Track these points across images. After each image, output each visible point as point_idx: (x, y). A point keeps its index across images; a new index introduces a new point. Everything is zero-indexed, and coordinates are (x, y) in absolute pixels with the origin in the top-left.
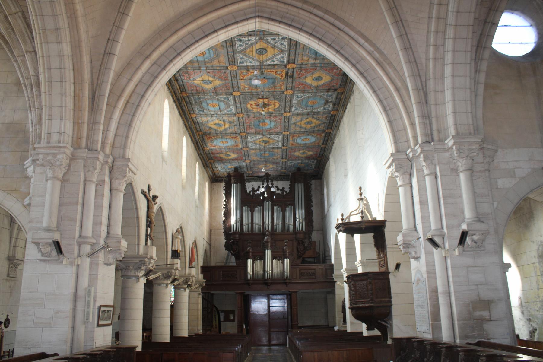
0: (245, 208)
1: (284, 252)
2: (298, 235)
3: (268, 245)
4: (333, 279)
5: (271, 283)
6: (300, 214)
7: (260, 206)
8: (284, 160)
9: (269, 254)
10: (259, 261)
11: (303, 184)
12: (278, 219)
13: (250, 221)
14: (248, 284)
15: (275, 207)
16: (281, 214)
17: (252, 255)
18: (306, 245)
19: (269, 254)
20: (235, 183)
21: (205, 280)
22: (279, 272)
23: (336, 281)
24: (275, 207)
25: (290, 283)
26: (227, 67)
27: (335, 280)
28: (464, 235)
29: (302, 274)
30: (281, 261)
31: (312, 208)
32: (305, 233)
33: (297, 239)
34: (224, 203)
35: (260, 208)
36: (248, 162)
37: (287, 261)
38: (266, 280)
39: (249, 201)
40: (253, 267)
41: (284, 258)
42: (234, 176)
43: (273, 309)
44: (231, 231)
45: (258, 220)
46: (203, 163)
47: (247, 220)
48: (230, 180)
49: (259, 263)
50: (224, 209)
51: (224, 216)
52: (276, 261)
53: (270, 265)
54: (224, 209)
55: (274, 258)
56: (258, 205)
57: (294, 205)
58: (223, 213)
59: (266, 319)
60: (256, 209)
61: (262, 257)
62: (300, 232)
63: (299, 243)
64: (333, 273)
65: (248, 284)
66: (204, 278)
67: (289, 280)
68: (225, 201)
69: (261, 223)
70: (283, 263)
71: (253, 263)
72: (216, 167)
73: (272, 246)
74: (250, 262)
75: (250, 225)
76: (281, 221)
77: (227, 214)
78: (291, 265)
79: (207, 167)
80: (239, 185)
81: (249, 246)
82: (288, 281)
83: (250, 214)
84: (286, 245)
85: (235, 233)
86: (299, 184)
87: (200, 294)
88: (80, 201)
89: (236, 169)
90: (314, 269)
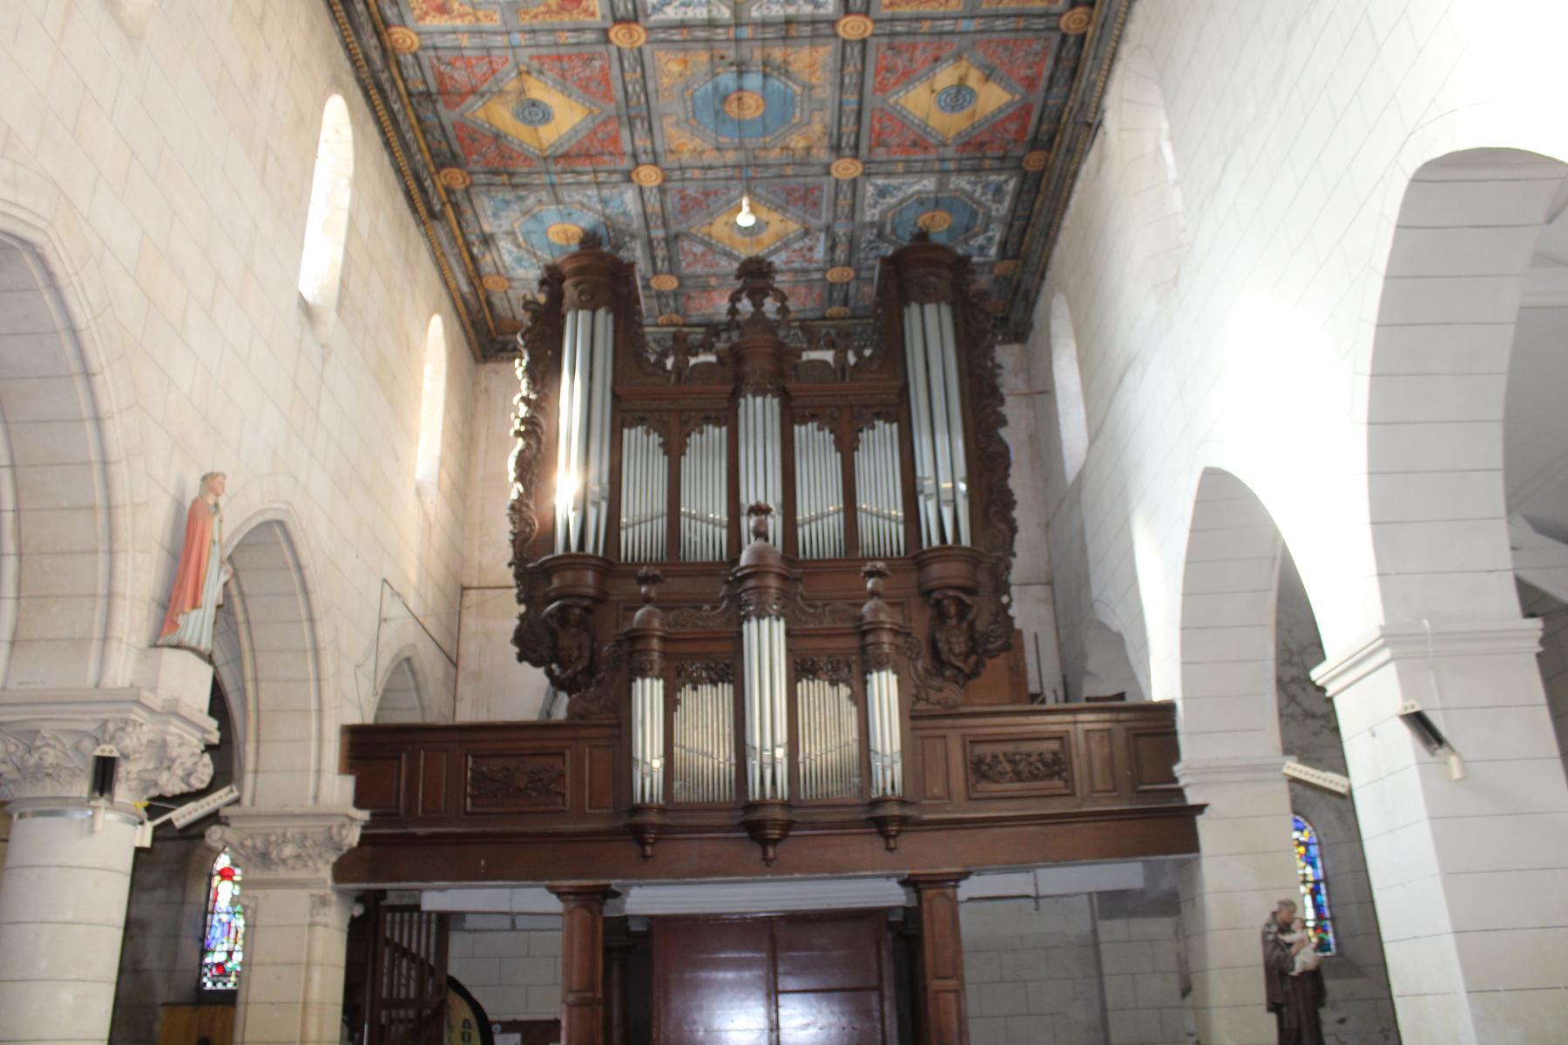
0: (634, 437)
1: (864, 631)
2: (936, 570)
3: (761, 590)
4: (1179, 792)
5: (788, 826)
6: (944, 466)
7: (717, 422)
8: (846, 169)
9: (766, 643)
10: (706, 690)
11: (946, 311)
12: (819, 501)
13: (660, 504)
14: (637, 833)
15: (800, 431)
16: (834, 461)
17: (664, 655)
18: (980, 626)
19: (766, 643)
20: (581, 305)
21: (364, 815)
22: (833, 757)
23: (1200, 808)
24: (800, 431)
25: (903, 821)
26: (606, 31)
27: (1192, 798)
28: (1419, 723)
29: (979, 770)
30: (844, 691)
31: (1004, 433)
32: (972, 558)
33: (926, 594)
34: (523, 410)
35: (716, 434)
36: (649, 176)
37: (885, 687)
38: (751, 807)
39: (657, 399)
40: (672, 736)
41: (866, 671)
42: (579, 272)
43: (778, 278)
44: (552, 548)
45: (705, 504)
46: (399, 171)
47: (643, 503)
48: (556, 298)
49: (706, 707)
50: (520, 443)
51: (520, 478)
52: (814, 691)
53: (781, 719)
54: (520, 443)
55: (800, 668)
56: (708, 420)
57: (898, 411)
58: (511, 462)
59: (786, 982)
60: (694, 438)
61: (728, 668)
62: (945, 552)
63: (941, 615)
64: (1173, 753)
65: (637, 833)
66: (359, 803)
67: (902, 802)
68: (525, 400)
69: (720, 513)
70: (861, 700)
71: (671, 704)
72: (487, 240)
73: (785, 597)
74: (649, 695)
75: (661, 525)
76: (833, 502)
77: (534, 467)
78: (914, 717)
79: (432, 215)
80: (604, 319)
81: (647, 600)
82: (895, 810)
83: (660, 464)
84: (874, 593)
85: (575, 561)
86: (930, 309)
87: (323, 902)
88: (314, 706)
89: (590, 240)
90: (1061, 738)
